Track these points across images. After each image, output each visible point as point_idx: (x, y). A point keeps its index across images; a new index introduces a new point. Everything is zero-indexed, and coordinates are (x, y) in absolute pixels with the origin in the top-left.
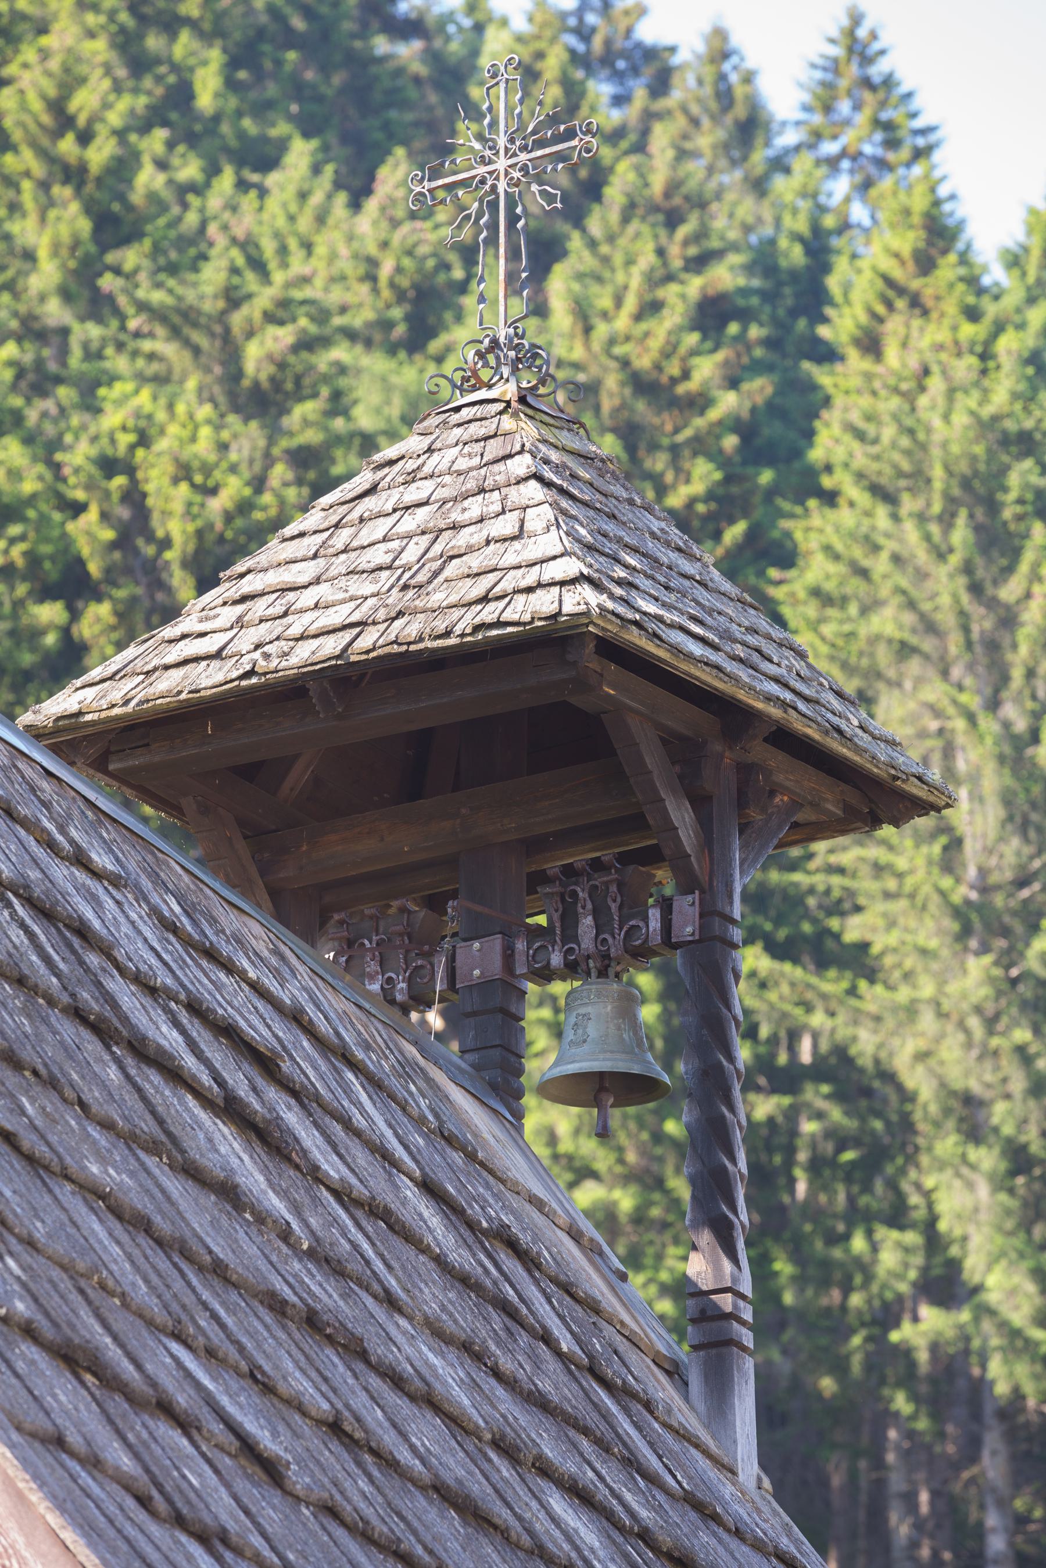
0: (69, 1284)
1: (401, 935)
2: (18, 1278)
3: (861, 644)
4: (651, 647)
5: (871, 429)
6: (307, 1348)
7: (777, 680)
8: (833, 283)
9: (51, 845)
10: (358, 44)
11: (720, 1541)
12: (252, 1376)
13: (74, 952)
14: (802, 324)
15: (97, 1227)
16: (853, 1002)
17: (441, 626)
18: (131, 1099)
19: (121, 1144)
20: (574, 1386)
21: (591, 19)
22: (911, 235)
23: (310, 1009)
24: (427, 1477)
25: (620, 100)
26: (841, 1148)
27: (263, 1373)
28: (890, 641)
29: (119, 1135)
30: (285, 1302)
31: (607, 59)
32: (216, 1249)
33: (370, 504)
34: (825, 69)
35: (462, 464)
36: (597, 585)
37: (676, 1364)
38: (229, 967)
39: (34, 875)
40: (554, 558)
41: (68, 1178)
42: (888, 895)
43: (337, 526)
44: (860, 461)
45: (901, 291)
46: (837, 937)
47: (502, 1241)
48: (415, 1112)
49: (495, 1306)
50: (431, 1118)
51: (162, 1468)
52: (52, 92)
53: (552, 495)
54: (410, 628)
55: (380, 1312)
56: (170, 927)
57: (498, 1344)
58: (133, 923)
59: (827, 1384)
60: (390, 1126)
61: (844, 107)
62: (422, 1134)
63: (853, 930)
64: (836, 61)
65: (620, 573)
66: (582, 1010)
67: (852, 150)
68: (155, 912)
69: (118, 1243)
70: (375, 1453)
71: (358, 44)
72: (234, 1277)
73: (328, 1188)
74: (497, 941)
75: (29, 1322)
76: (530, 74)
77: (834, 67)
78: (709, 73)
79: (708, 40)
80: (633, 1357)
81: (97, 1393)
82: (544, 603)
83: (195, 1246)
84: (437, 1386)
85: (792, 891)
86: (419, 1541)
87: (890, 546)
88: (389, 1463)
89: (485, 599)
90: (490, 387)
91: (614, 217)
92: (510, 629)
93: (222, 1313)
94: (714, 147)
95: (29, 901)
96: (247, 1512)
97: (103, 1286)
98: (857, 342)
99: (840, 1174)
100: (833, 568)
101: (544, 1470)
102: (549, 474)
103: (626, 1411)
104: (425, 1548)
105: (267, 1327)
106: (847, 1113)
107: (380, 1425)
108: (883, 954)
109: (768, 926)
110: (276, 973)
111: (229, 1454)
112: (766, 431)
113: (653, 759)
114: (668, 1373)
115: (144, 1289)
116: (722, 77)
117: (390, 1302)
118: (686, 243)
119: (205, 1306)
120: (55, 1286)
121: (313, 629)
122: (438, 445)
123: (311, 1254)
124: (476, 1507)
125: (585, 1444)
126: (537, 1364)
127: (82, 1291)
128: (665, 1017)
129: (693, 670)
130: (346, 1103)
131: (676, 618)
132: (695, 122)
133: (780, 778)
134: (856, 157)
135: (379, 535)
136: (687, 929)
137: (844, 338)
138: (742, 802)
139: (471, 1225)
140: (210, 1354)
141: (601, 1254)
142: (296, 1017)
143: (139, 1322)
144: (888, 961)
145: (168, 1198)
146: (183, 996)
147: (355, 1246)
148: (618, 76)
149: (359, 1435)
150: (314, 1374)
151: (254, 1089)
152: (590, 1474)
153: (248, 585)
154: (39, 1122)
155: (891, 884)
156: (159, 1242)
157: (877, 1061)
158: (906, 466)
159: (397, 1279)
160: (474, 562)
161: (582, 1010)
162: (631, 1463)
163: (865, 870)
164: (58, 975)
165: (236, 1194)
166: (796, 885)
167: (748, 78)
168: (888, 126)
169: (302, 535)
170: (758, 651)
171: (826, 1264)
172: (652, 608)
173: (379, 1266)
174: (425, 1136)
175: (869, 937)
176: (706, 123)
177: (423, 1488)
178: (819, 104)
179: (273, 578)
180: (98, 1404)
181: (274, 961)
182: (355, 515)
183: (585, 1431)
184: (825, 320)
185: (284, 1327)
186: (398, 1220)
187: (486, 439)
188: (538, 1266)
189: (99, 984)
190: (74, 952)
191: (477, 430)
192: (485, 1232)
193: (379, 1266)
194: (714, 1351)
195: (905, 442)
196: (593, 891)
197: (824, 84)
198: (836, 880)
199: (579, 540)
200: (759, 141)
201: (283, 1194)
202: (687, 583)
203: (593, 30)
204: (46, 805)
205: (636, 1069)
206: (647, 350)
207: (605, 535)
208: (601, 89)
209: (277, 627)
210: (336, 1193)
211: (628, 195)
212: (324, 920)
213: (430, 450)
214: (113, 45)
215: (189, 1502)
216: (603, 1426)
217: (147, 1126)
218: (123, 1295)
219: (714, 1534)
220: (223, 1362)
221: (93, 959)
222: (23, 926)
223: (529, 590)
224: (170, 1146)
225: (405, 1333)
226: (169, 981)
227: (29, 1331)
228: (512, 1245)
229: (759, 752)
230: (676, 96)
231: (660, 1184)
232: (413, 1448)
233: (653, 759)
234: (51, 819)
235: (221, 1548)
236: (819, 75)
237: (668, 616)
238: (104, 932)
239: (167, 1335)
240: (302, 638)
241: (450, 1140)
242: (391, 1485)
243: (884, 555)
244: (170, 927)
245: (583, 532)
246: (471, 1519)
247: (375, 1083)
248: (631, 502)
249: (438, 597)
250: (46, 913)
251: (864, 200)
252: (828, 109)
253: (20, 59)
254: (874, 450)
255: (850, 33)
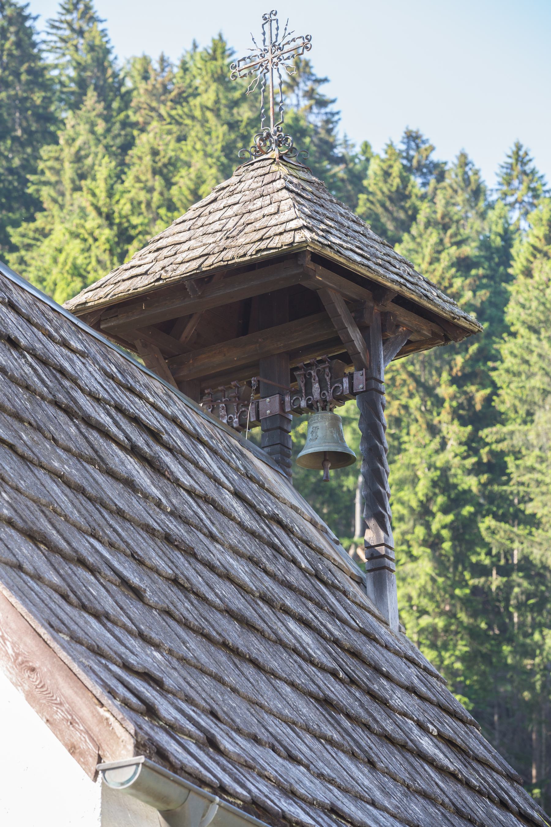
0: (37, 508)
1: (235, 397)
2: (8, 502)
3: (527, 392)
4: (336, 257)
5: (527, 304)
6: (164, 549)
7: (397, 274)
8: (513, 251)
9: (50, 336)
10: (317, 165)
11: (377, 649)
12: (133, 556)
13: (57, 379)
14: (502, 269)
15: (55, 488)
16: (530, 537)
17: (242, 252)
18: (81, 441)
19: (75, 459)
20: (307, 582)
21: (412, 153)
22: (543, 229)
23: (182, 418)
24: (222, 606)
25: (424, 184)
26: (528, 598)
27: (138, 555)
28: (539, 389)
29: (74, 455)
30: (154, 529)
31: (419, 168)
32: (118, 504)
33: (214, 206)
34: (507, 168)
35: (254, 186)
36: (310, 230)
37: (361, 579)
38: (140, 396)
39: (38, 346)
40: (292, 220)
41: (42, 467)
42: (543, 494)
43: (199, 216)
44: (524, 317)
45: (540, 251)
46: (523, 512)
47: (275, 521)
48: (234, 465)
49: (268, 546)
50: (242, 468)
51: (77, 586)
52: (192, 187)
53: (293, 195)
54: (228, 255)
55: (206, 541)
56: (110, 376)
57: (268, 560)
58: (90, 372)
59: (527, 695)
60: (220, 469)
61: (516, 183)
62: (236, 474)
63: (529, 509)
64: (511, 165)
65: (323, 226)
66: (315, 425)
67: (519, 200)
68: (102, 369)
69: (66, 495)
70: (196, 594)
71: (317, 165)
72: (128, 517)
73: (185, 489)
74: (277, 398)
75: (10, 519)
76: (387, 174)
77: (511, 167)
78: (460, 171)
79: (458, 158)
80: (339, 574)
81: (46, 553)
82: (287, 238)
83: (108, 501)
84: (233, 572)
85: (503, 493)
86: (215, 630)
87: (537, 350)
88: (203, 599)
89: (261, 239)
90: (267, 153)
91: (422, 227)
92: (272, 251)
93: (120, 530)
94: (463, 201)
95: (35, 356)
96: (121, 608)
97: (55, 511)
98: (523, 273)
99: (528, 609)
100: (514, 361)
101: (286, 611)
102: (291, 187)
103: (334, 594)
104: (217, 633)
105: (143, 538)
106: (530, 584)
107: (200, 584)
108: (542, 517)
109: (495, 509)
110: (166, 402)
111: (115, 585)
112: (488, 312)
113: (341, 309)
114: (358, 583)
115: (77, 514)
116: (465, 173)
117: (212, 537)
118: (451, 237)
119: (111, 526)
120: (28, 508)
121: (186, 259)
122: (243, 179)
123: (172, 513)
124: (247, 621)
125: (310, 604)
126: (288, 570)
127: (43, 512)
128: (454, 547)
129: (357, 268)
130: (197, 457)
131: (349, 246)
132: (456, 191)
133: (402, 319)
134: (522, 202)
135: (217, 218)
136: (360, 386)
137: (518, 271)
138: (383, 329)
139: (259, 513)
140: (111, 545)
141: (327, 532)
142: (174, 420)
143: (73, 528)
144: (544, 520)
145: (97, 482)
146: (112, 403)
147: (196, 513)
148: (423, 175)
149: (186, 585)
150: (166, 559)
151: (148, 445)
152: (311, 615)
153: (159, 244)
154: (29, 443)
155: (544, 489)
156: (90, 499)
157: (542, 562)
158: (542, 318)
159: (217, 529)
160: (258, 225)
161: (315, 425)
162: (333, 614)
163: (533, 484)
164: (47, 387)
165: (133, 485)
166: (505, 491)
167: (476, 173)
168: (534, 190)
169: (184, 221)
170: (389, 262)
171: (524, 645)
172: (338, 241)
173: (207, 522)
174: (239, 476)
175: (536, 511)
176: (460, 192)
177: (221, 611)
178: (505, 182)
179: (171, 240)
180: (46, 557)
181: (165, 398)
182: (207, 211)
183: (310, 599)
184: (511, 266)
185: (153, 540)
186: (219, 505)
187: (265, 175)
188: (293, 533)
189: (68, 393)
190: (57, 379)
191: (261, 171)
192: (266, 516)
193: (207, 522)
194: (377, 572)
195: (542, 308)
196: (318, 372)
197: (507, 174)
198: (521, 488)
199: (304, 213)
200: (482, 198)
201: (161, 489)
202: (356, 234)
203: (413, 157)
204: (50, 321)
205: (340, 450)
206: (435, 276)
207: (318, 213)
208: (416, 181)
209: (171, 260)
210: (189, 492)
211: (427, 218)
212: (202, 394)
213: (240, 182)
214: (219, 170)
215: (89, 600)
216: (320, 598)
217: (89, 452)
218: (65, 516)
219: (374, 646)
220: (118, 549)
221: (67, 383)
222: (31, 366)
223: (281, 234)
224: (99, 460)
225: (218, 550)
226: (106, 396)
227: (10, 523)
228: (279, 523)
229: (390, 307)
230: (448, 181)
231: (454, 616)
232: (216, 595)
233: (341, 309)
234: (52, 326)
235: (105, 621)
236: (505, 170)
237: (345, 245)
238: (73, 372)
239: (88, 535)
240: (182, 263)
241: (251, 478)
242: (204, 609)
243: (535, 354)
244: (110, 376)
245: (306, 210)
246: (245, 626)
247: (214, 452)
248: (331, 201)
249: (241, 240)
250: (44, 362)
251: (526, 219)
252: (509, 184)
253: (179, 174)
254: (529, 312)
255: (517, 153)
